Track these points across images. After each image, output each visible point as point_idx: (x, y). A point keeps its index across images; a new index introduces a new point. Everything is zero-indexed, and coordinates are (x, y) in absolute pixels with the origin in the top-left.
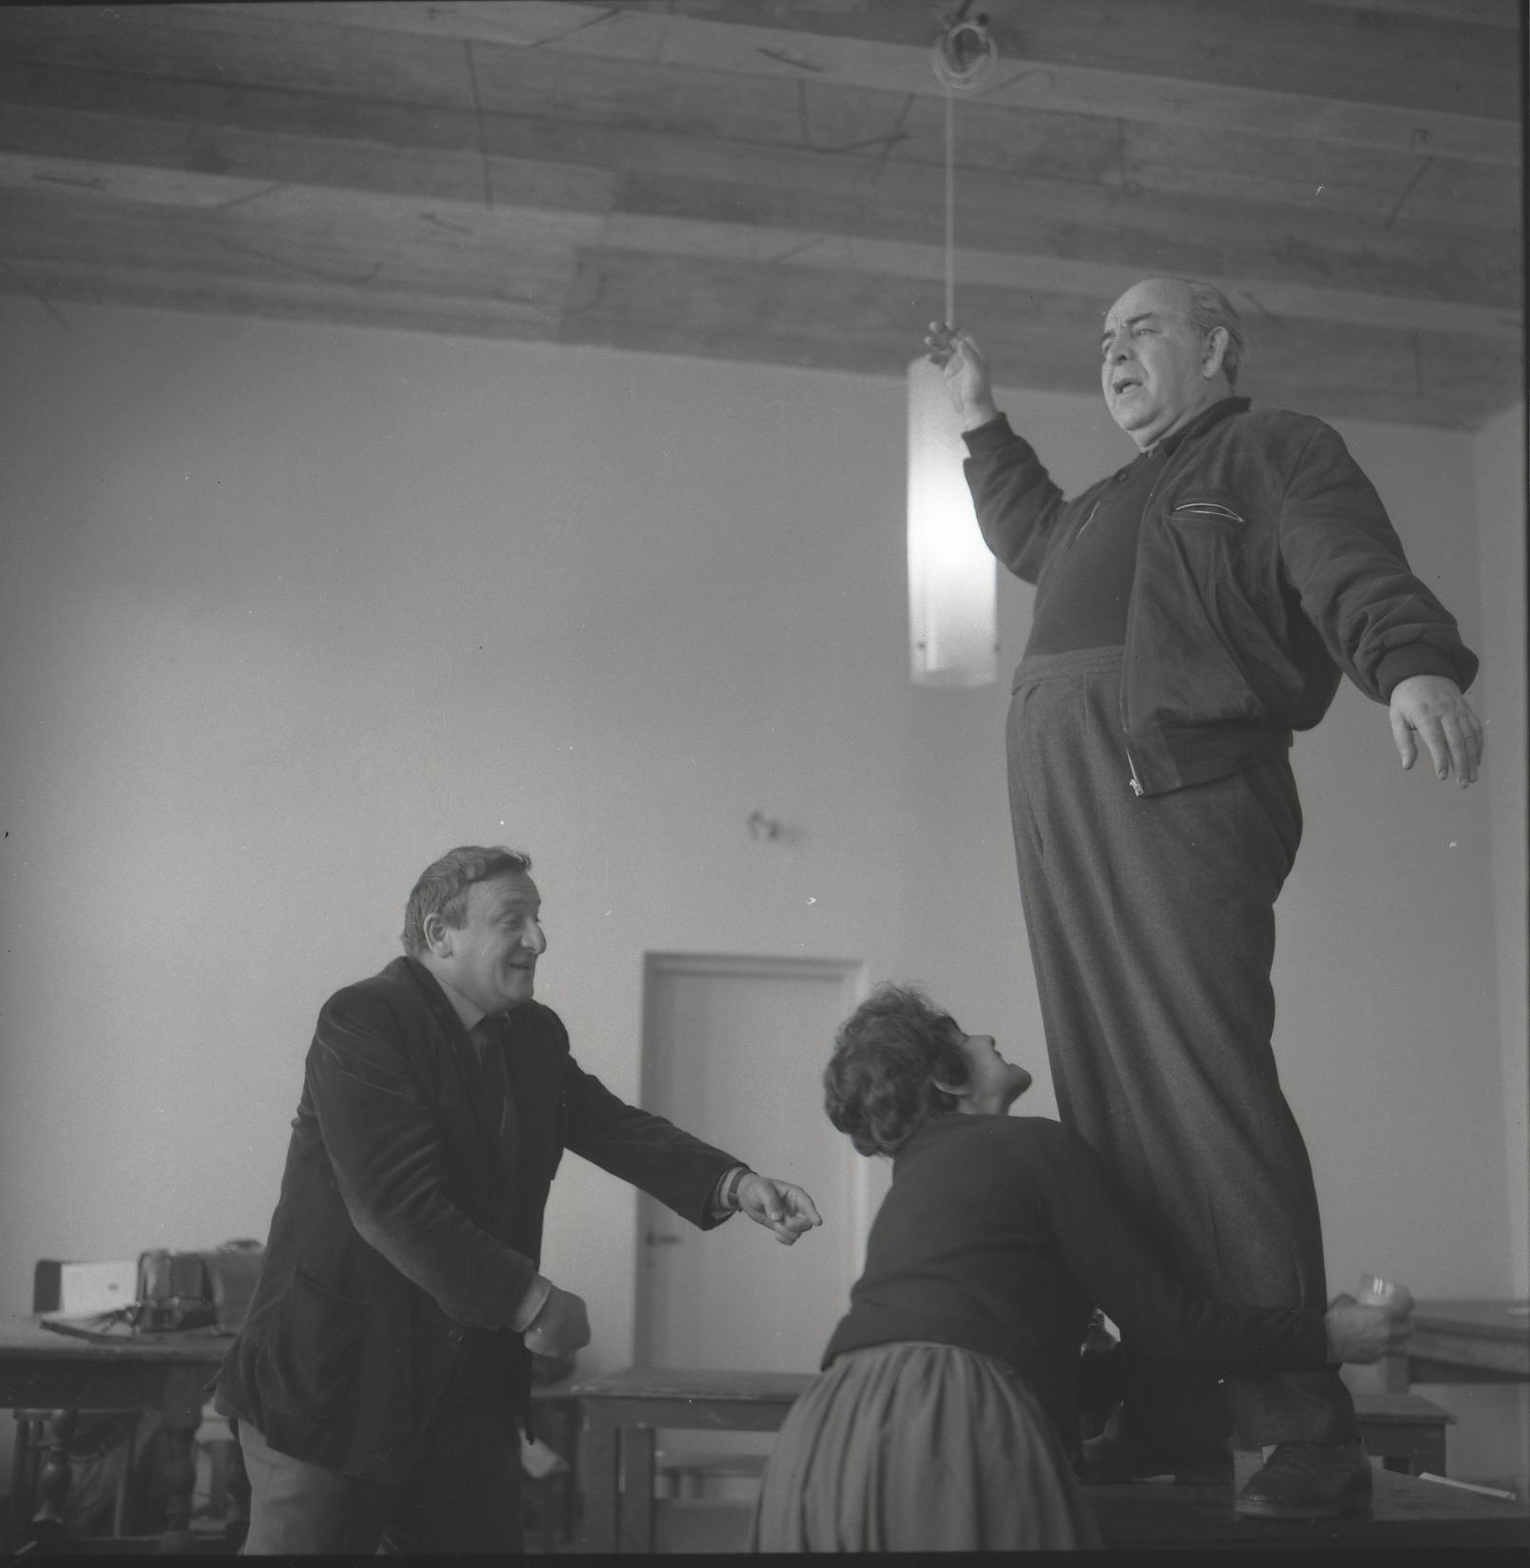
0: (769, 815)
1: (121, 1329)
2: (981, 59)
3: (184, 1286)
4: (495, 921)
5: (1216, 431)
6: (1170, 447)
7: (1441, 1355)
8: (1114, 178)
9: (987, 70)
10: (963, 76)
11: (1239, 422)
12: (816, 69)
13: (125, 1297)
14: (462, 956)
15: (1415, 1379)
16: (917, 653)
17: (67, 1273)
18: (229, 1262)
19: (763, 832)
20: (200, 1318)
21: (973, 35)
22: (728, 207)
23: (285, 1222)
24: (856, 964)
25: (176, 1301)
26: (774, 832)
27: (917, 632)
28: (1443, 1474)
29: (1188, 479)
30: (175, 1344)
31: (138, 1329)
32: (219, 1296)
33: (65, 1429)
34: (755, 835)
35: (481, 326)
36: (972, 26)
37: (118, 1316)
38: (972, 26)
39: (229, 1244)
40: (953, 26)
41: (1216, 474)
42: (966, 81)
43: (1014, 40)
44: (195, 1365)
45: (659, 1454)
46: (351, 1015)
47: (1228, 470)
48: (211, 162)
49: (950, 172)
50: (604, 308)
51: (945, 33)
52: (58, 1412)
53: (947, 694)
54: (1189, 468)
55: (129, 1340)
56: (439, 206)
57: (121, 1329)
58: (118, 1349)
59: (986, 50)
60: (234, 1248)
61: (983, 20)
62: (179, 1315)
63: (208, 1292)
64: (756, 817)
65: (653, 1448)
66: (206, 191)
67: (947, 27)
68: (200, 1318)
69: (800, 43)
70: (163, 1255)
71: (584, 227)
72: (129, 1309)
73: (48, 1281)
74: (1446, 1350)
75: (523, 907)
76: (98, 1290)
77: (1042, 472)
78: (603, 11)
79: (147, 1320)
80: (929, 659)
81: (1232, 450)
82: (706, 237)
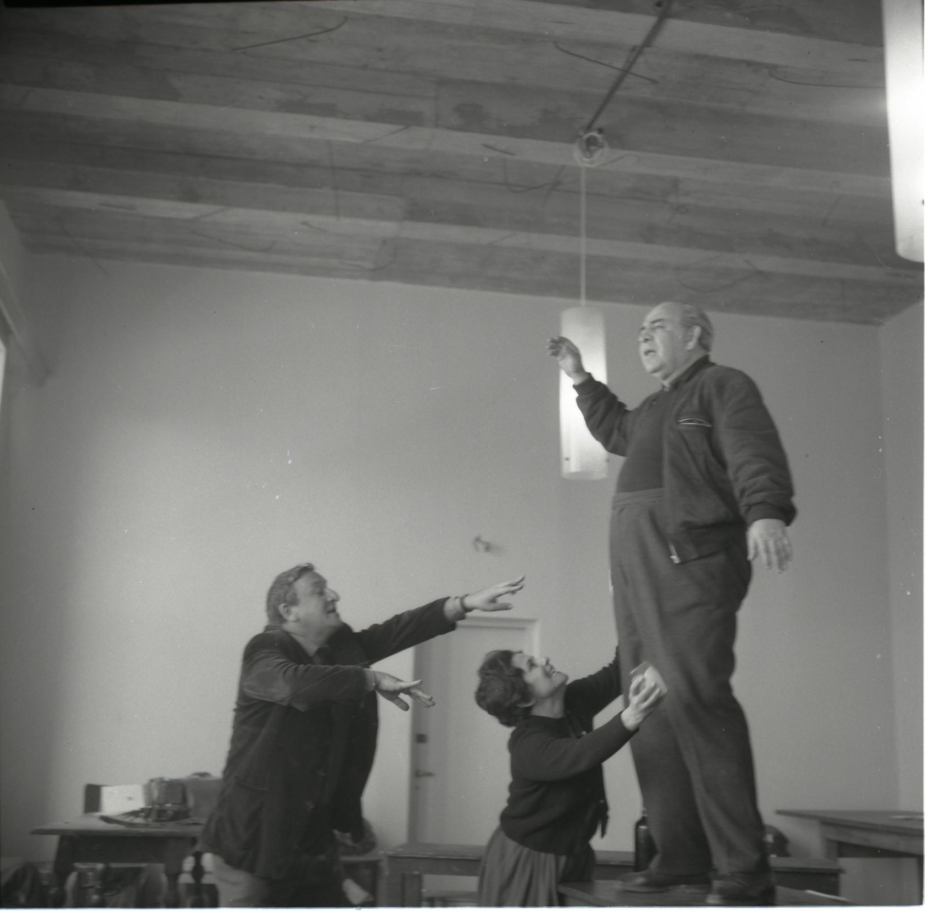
0: (485, 539)
1: (139, 820)
2: (600, 152)
3: (172, 798)
4: (312, 594)
5: (695, 378)
6: (676, 385)
7: (853, 841)
8: (672, 199)
9: (603, 157)
10: (588, 160)
11: (709, 370)
12: (513, 154)
13: (139, 803)
14: (303, 616)
15: (841, 855)
16: (565, 463)
17: (106, 792)
18: (200, 781)
19: (481, 547)
20: (178, 816)
21: (595, 138)
22: (465, 218)
23: (233, 760)
24: (531, 621)
25: (169, 805)
26: (488, 548)
27: (565, 454)
28: (836, 894)
29: (683, 406)
30: (170, 828)
31: (150, 820)
32: (191, 802)
33: (104, 876)
34: (477, 549)
35: (328, 272)
36: (595, 134)
37: (135, 814)
38: (595, 134)
39: (195, 774)
40: (586, 133)
41: (696, 401)
42: (591, 163)
43: (617, 139)
44: (178, 838)
45: (424, 890)
46: (256, 650)
47: (701, 398)
48: (192, 197)
49: (583, 198)
50: (394, 264)
51: (580, 137)
52: (100, 866)
53: (579, 485)
54: (683, 400)
55: (146, 826)
56: (310, 218)
57: (139, 820)
58: (143, 830)
59: (602, 146)
60: (197, 777)
61: (600, 131)
62: (170, 813)
63: (184, 800)
64: (478, 539)
65: (421, 887)
66: (187, 211)
67: (581, 133)
68: (180, 815)
69: (504, 142)
70: (161, 781)
71: (388, 228)
72: (142, 810)
73: (93, 796)
74: (856, 838)
75: (320, 585)
76: (122, 800)
77: (614, 397)
78: (400, 127)
79: (154, 815)
80: (572, 466)
81: (702, 388)
82: (456, 233)
